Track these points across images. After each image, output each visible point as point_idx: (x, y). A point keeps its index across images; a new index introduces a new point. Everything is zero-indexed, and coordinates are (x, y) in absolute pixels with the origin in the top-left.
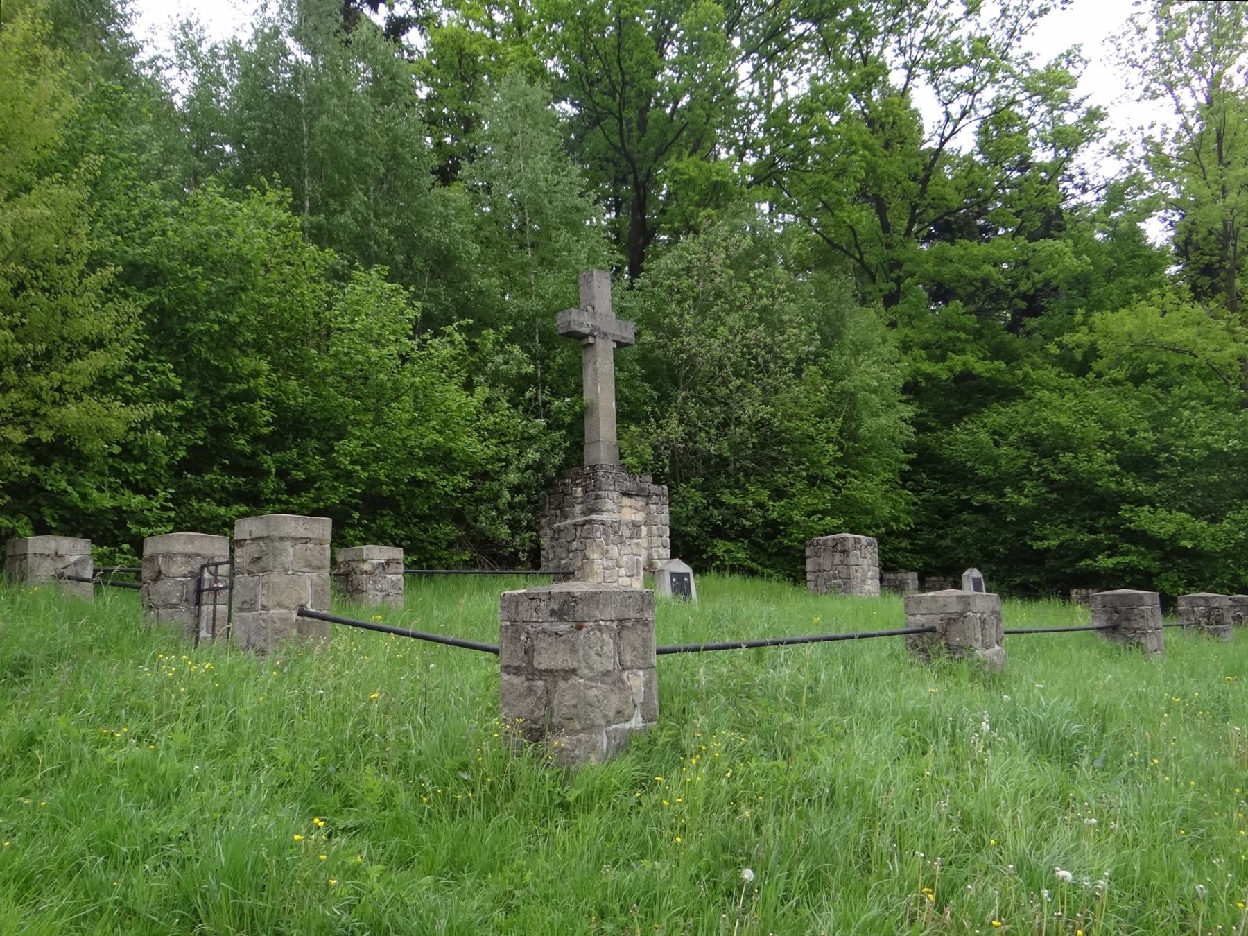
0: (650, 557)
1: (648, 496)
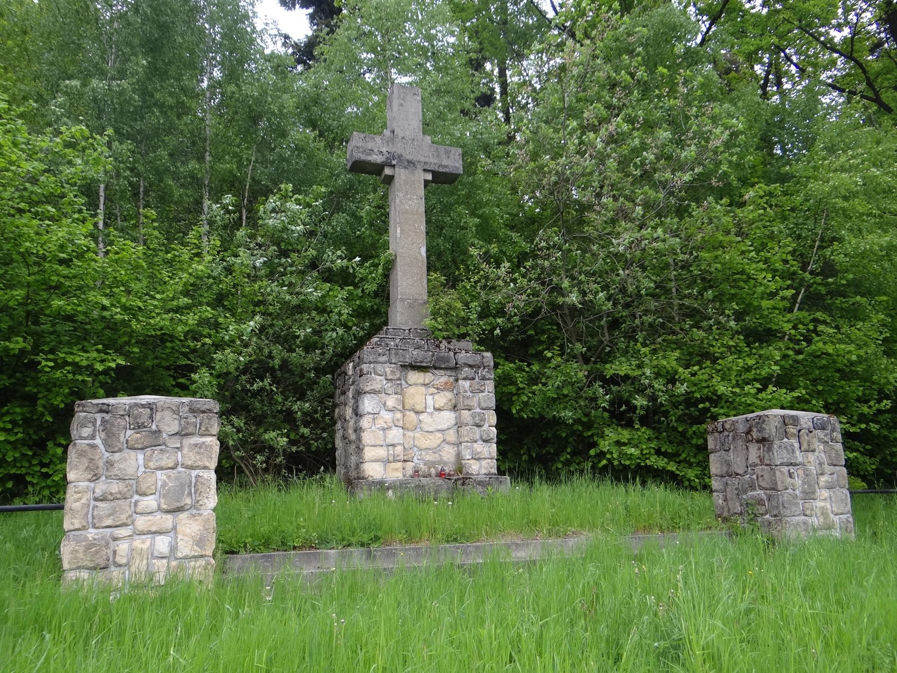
0: (459, 457)
1: (456, 368)
